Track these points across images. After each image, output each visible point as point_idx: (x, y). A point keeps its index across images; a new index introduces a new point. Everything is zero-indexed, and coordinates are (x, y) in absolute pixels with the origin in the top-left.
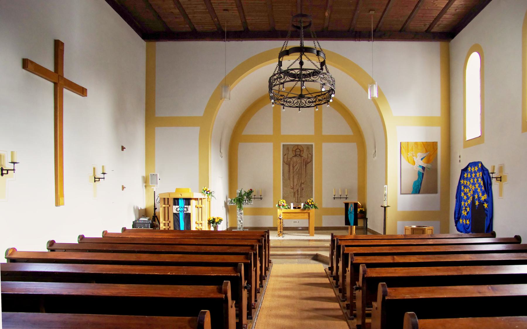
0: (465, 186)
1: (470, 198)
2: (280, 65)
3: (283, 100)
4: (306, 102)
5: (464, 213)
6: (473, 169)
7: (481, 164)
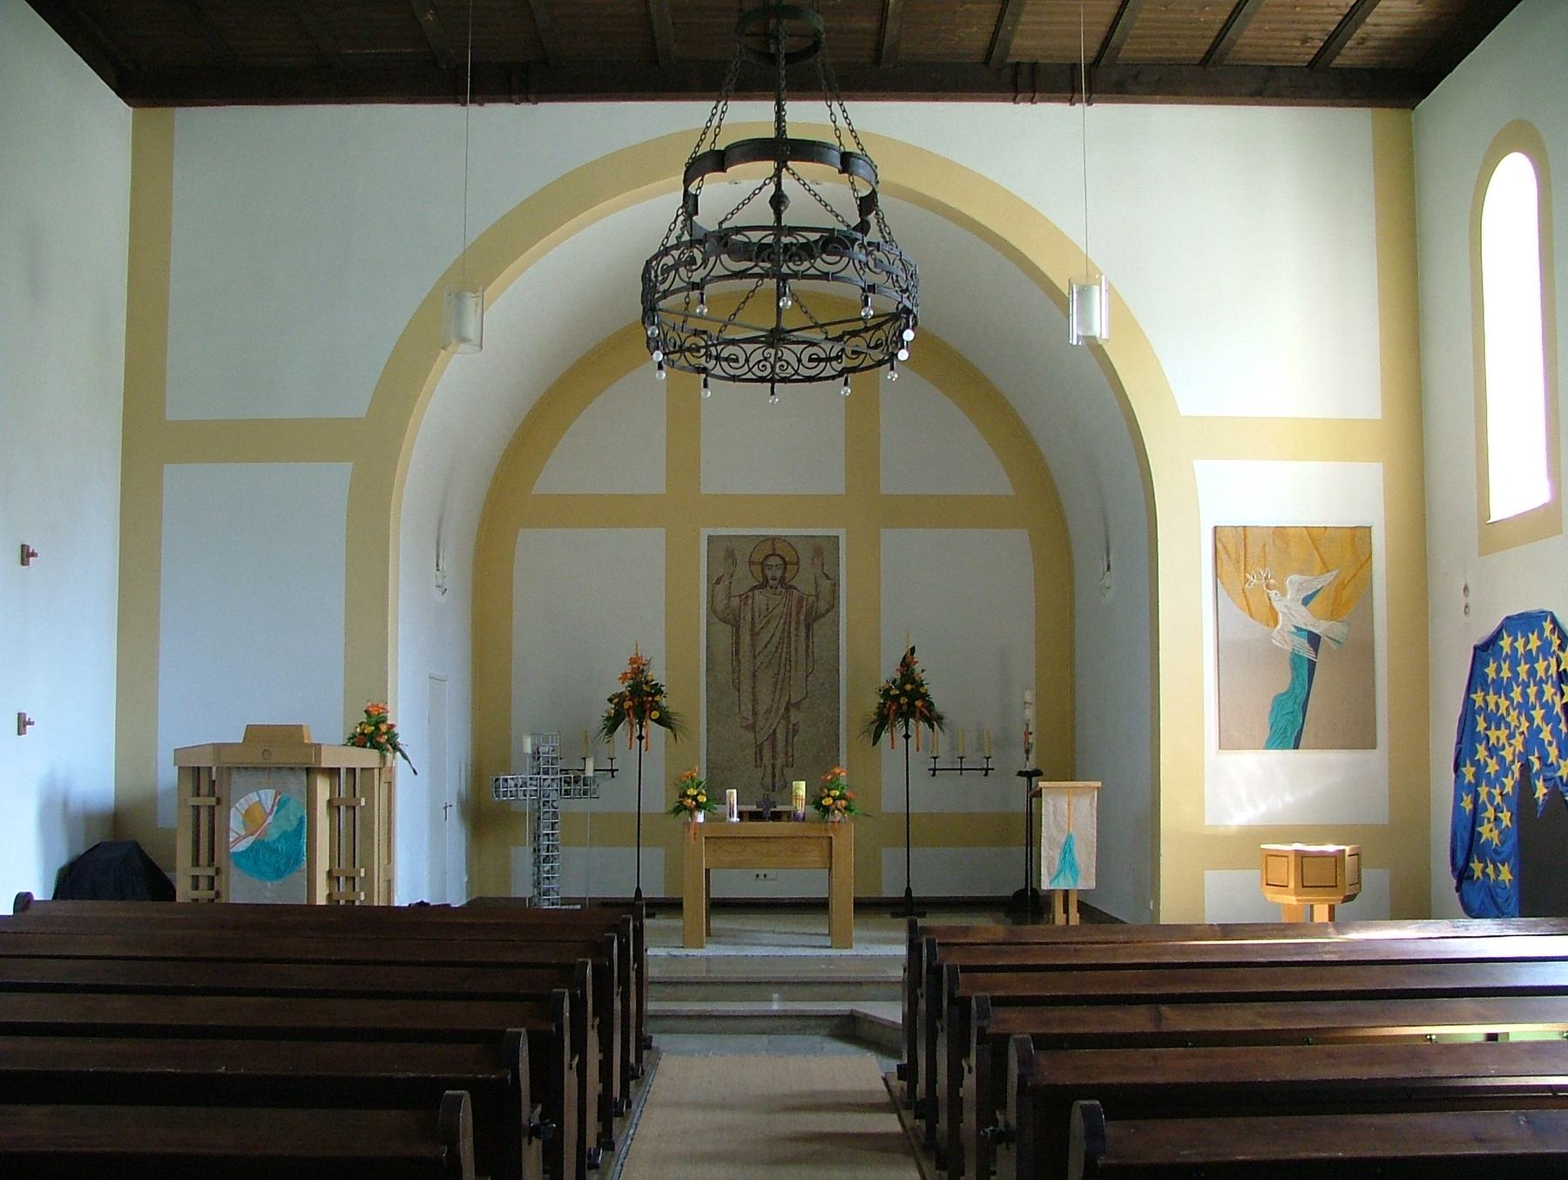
0: (1496, 720)
1: (1513, 767)
2: (690, 209)
3: (703, 351)
4: (799, 361)
5: (1487, 832)
6: (1520, 644)
7: (1554, 621)
